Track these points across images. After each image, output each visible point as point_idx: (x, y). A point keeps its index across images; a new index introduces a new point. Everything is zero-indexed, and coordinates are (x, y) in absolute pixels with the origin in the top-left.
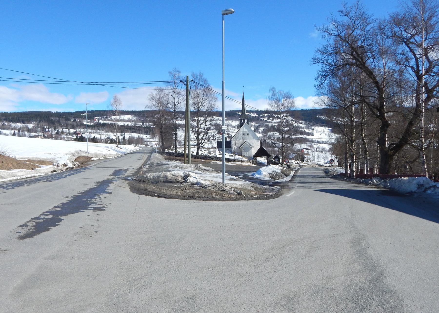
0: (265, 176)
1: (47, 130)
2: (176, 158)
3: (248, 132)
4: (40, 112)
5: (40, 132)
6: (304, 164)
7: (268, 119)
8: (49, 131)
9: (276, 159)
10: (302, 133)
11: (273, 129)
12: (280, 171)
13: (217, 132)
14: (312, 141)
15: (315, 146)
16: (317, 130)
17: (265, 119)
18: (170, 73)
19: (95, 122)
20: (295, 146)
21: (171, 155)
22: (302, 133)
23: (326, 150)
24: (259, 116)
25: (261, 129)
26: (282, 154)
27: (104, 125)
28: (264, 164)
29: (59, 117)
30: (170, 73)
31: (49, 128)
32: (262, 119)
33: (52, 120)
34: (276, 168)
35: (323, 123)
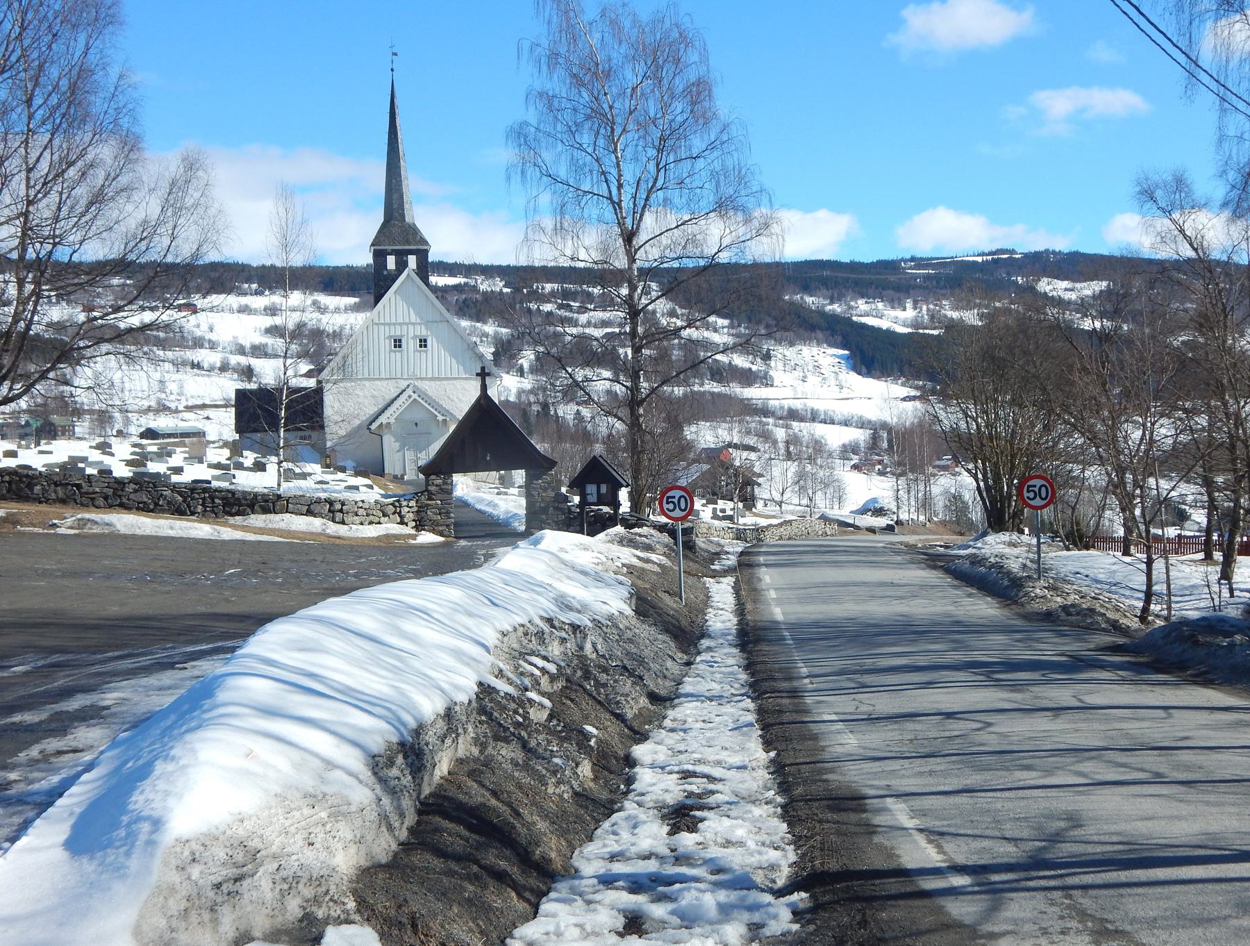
3: (422, 331)
6: (763, 522)
7: (560, 307)
9: (591, 489)
10: (721, 374)
11: (587, 353)
12: (614, 602)
14: (765, 412)
15: (780, 434)
16: (785, 359)
17: (547, 307)
22: (721, 374)
23: (830, 455)
25: (527, 358)
32: (533, 306)
34: (585, 559)
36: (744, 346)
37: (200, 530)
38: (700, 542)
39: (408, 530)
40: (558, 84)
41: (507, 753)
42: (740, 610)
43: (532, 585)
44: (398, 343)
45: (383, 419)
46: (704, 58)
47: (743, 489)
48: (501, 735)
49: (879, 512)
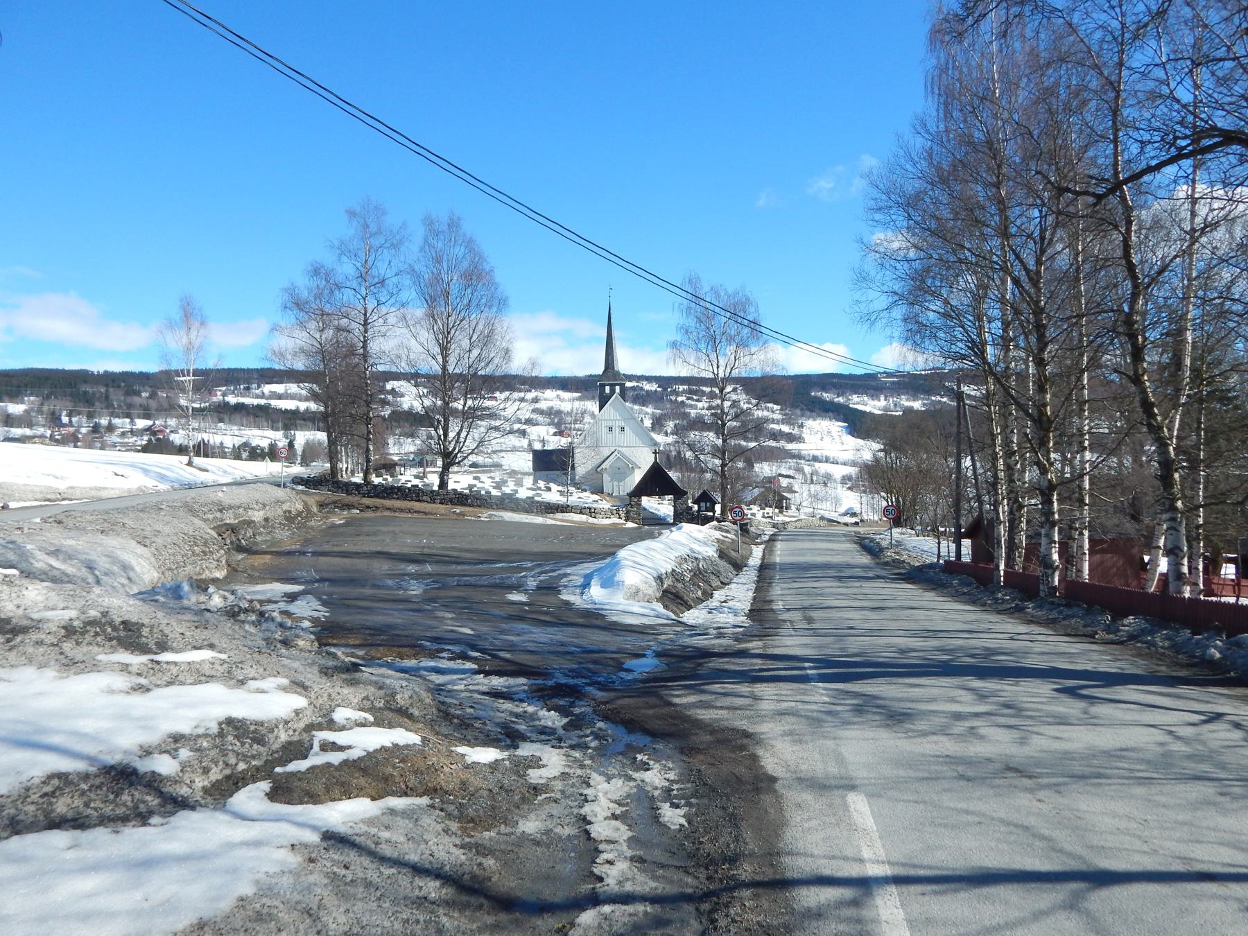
0: (635, 594)
1: (65, 419)
2: (366, 501)
4: (64, 371)
5: (44, 426)
6: (787, 519)
7: (688, 398)
8: (70, 424)
9: (703, 504)
11: (699, 424)
12: (711, 552)
13: (552, 430)
14: (799, 456)
15: (807, 469)
16: (811, 429)
17: (680, 399)
18: (352, 214)
19: (214, 399)
20: (756, 469)
21: (348, 493)
24: (665, 389)
25: (670, 425)
26: (723, 489)
27: (240, 408)
28: (664, 519)
29: (107, 386)
30: (352, 214)
31: (70, 415)
32: (673, 398)
33: (85, 393)
34: (700, 536)
35: (827, 411)
36: (787, 421)
37: (539, 520)
38: (752, 529)
39: (622, 521)
40: (692, 322)
41: (679, 585)
42: (763, 558)
43: (682, 545)
44: (611, 429)
45: (603, 466)
46: (757, 310)
47: (780, 503)
48: (678, 581)
49: (854, 515)
